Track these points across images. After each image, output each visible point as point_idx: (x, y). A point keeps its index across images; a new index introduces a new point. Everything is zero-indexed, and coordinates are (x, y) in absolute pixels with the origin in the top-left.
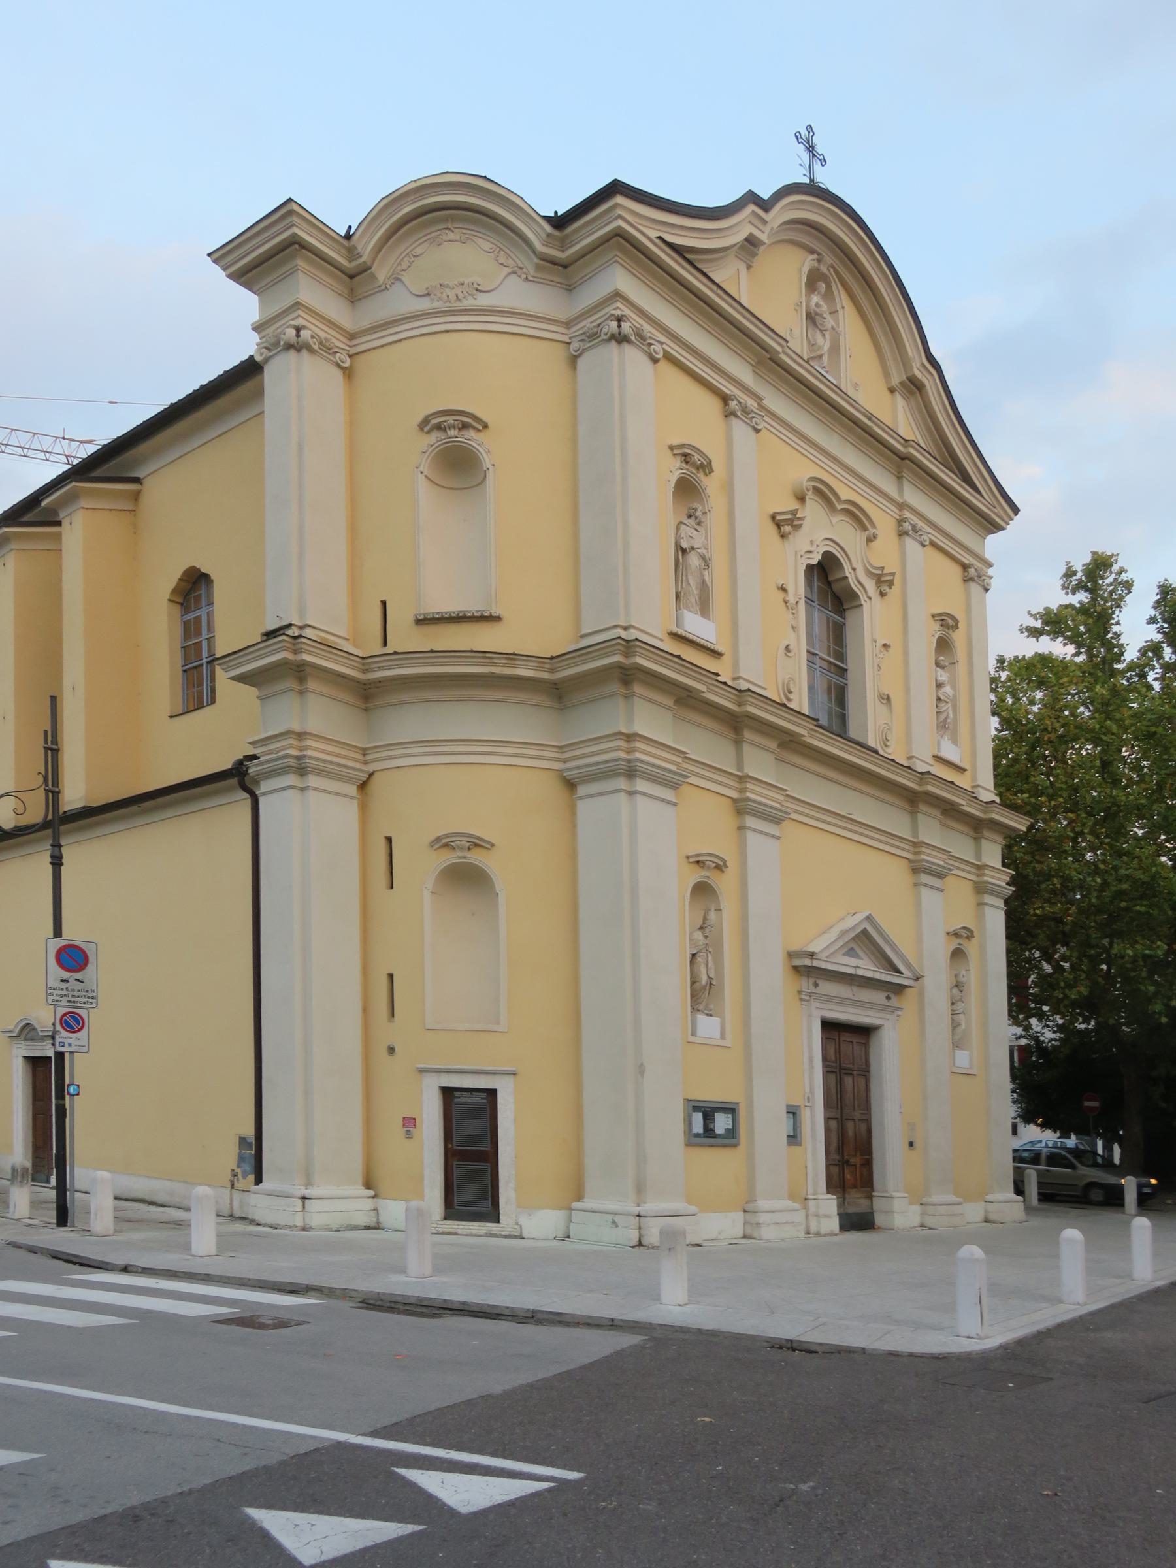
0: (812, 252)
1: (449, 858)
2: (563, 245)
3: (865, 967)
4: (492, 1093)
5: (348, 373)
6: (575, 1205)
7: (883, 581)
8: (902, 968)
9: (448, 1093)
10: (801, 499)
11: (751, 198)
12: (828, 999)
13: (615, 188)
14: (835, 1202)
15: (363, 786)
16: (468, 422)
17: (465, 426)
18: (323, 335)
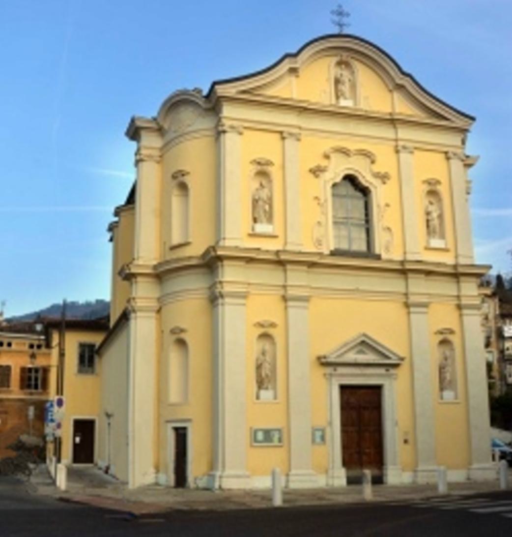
1: (261, 331)
2: (210, 102)
3: (370, 357)
7: (383, 178)
8: (391, 355)
9: (176, 429)
10: (327, 157)
12: (342, 375)
13: (215, 84)
15: (159, 311)
16: (183, 174)
17: (183, 175)
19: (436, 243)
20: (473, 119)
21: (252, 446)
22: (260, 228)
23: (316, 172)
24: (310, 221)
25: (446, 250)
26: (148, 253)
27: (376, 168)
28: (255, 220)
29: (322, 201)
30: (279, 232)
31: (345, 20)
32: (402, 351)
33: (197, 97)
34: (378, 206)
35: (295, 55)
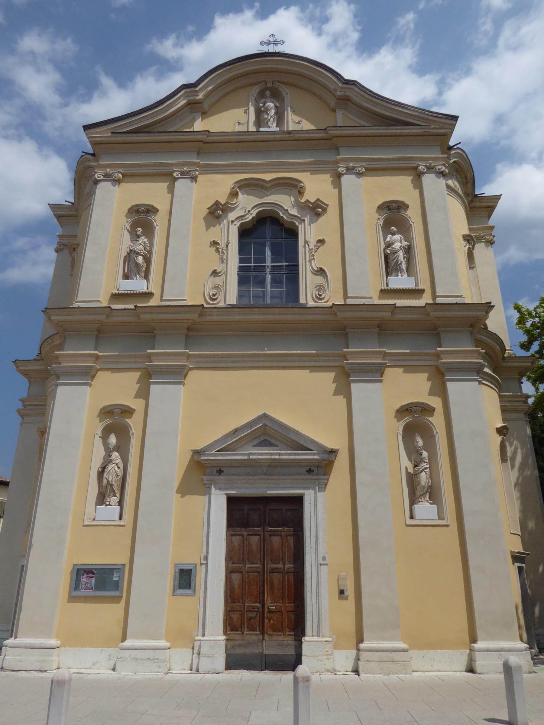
0: (260, 83)
7: (317, 209)
14: (224, 643)
20: (455, 118)
23: (216, 213)
29: (222, 246)
32: (327, 436)
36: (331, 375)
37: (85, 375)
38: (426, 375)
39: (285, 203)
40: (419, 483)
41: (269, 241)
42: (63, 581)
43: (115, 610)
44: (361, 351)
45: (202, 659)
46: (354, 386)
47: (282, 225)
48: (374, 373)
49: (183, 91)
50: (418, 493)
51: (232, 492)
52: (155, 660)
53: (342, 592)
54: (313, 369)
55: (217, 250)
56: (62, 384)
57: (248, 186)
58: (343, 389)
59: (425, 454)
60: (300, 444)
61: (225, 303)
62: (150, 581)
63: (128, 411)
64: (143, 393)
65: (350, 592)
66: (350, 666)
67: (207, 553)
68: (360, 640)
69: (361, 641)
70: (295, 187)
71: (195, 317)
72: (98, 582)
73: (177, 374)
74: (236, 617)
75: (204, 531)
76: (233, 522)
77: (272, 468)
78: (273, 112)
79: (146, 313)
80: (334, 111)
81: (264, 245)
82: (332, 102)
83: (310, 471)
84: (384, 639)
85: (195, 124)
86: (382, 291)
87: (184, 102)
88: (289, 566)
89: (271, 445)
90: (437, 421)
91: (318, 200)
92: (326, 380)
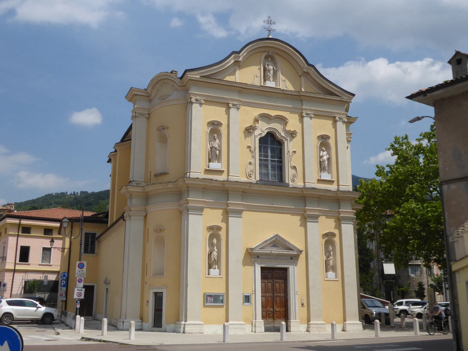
4: (162, 293)
5: (148, 118)
6: (177, 323)
7: (292, 134)
9: (156, 293)
11: (234, 53)
13: (186, 71)
18: (141, 112)
19: (325, 176)
20: (354, 95)
21: (205, 306)
22: (215, 165)
23: (249, 131)
24: (243, 164)
25: (331, 182)
26: (137, 171)
27: (288, 128)
28: (210, 161)
29: (253, 149)
30: (225, 169)
31: (273, 27)
32: (301, 246)
33: (174, 78)
34: (288, 151)
35: (239, 53)
36: (299, 218)
37: (200, 210)
38: (333, 220)
39: (277, 127)
40: (329, 264)
41: (272, 146)
42: (201, 299)
43: (223, 310)
44: (312, 209)
45: (256, 328)
46: (308, 223)
47: (275, 138)
48: (315, 218)
49: (233, 56)
50: (328, 268)
51: (263, 266)
52: (242, 328)
53: (303, 304)
54: (292, 214)
55: (250, 150)
56: (191, 214)
57: (266, 117)
58: (304, 225)
59: (332, 253)
60: (289, 248)
61: (255, 179)
62: (235, 299)
63: (219, 228)
64: (226, 220)
65: (305, 304)
66: (305, 329)
67: (255, 289)
68: (345, 320)
69: (310, 321)
70: (283, 120)
71: (247, 187)
72: (214, 300)
73: (238, 213)
74: (264, 313)
75: (248, 280)
76: (264, 277)
77: (278, 257)
78: (272, 72)
79: (227, 184)
80: (300, 76)
81: (267, 148)
82: (300, 73)
83: (291, 258)
84: (317, 320)
85: (236, 73)
86: (318, 180)
87: (233, 61)
88: (282, 295)
89: (277, 247)
90: (337, 239)
91: (295, 131)
92: (297, 219)
